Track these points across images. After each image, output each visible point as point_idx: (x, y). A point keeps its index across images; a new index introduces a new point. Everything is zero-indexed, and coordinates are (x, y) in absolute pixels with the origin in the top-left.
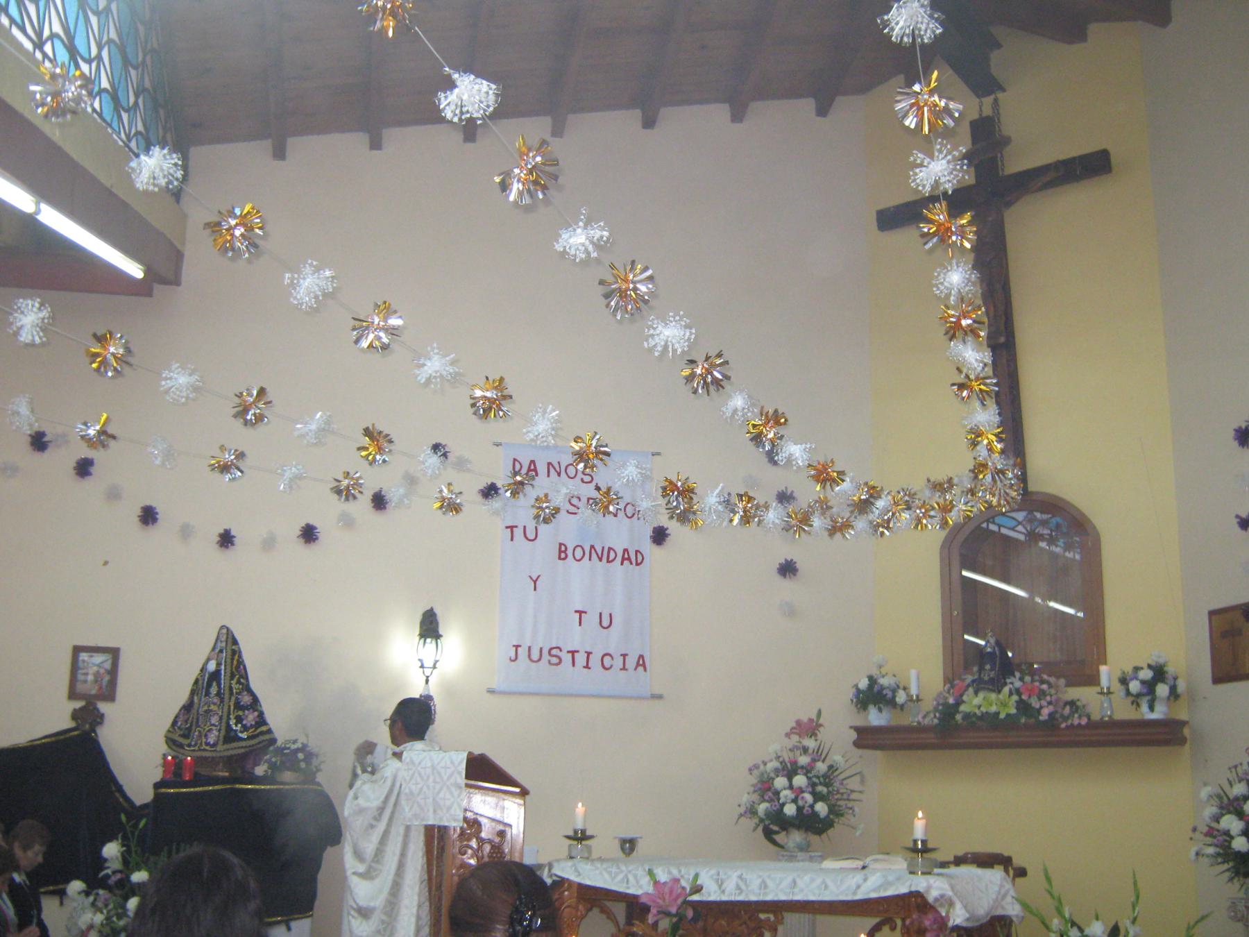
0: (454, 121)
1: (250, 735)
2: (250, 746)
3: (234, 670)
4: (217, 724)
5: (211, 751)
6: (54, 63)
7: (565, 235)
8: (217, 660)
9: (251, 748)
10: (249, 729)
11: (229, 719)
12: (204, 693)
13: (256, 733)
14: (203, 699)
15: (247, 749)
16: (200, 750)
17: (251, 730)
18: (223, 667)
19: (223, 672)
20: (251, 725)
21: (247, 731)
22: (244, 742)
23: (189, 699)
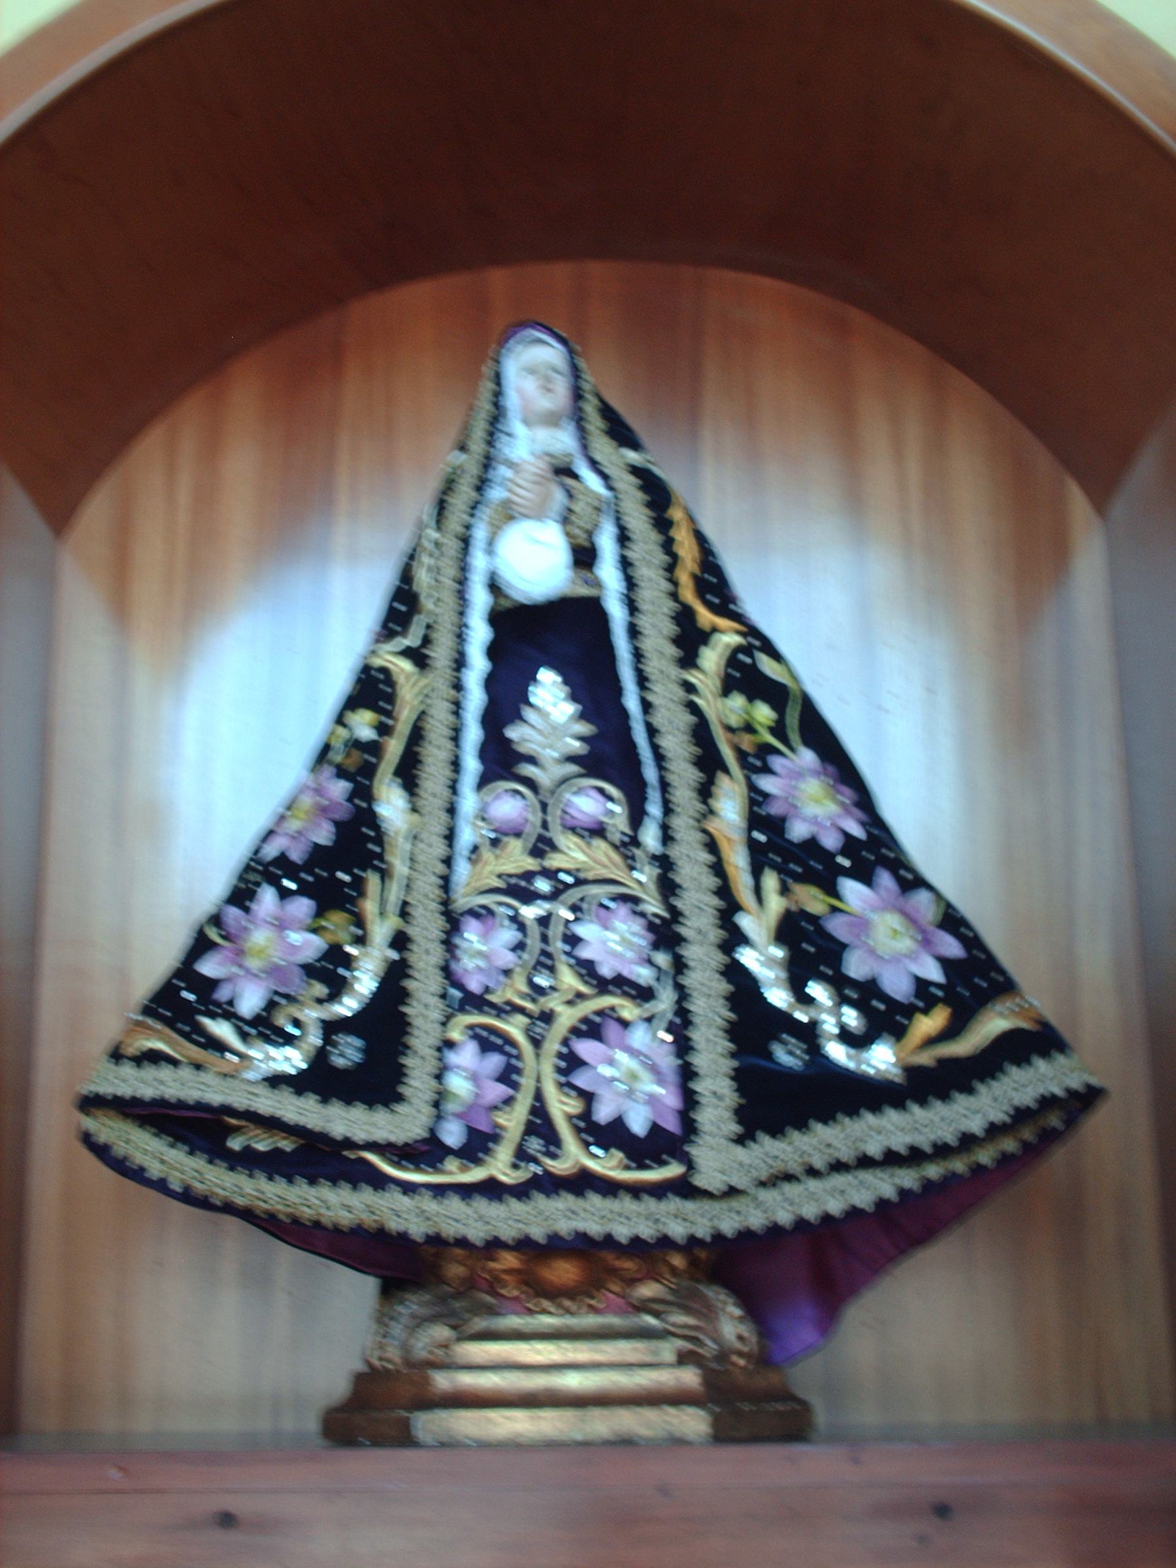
0: (339, 1062)
1: (926, 1059)
2: (942, 1151)
3: (688, 594)
4: (643, 975)
5: (636, 1190)
6: (508, 1048)
7: (243, 1073)
8: (566, 520)
9: (933, 1171)
10: (909, 1011)
11: (734, 938)
12: (472, 765)
13: (962, 1047)
14: (469, 801)
15: (908, 1178)
16: (550, 1184)
17: (928, 1024)
18: (608, 572)
19: (616, 611)
20: (922, 985)
21: (898, 1033)
22: (892, 1117)
23: (656, 964)
